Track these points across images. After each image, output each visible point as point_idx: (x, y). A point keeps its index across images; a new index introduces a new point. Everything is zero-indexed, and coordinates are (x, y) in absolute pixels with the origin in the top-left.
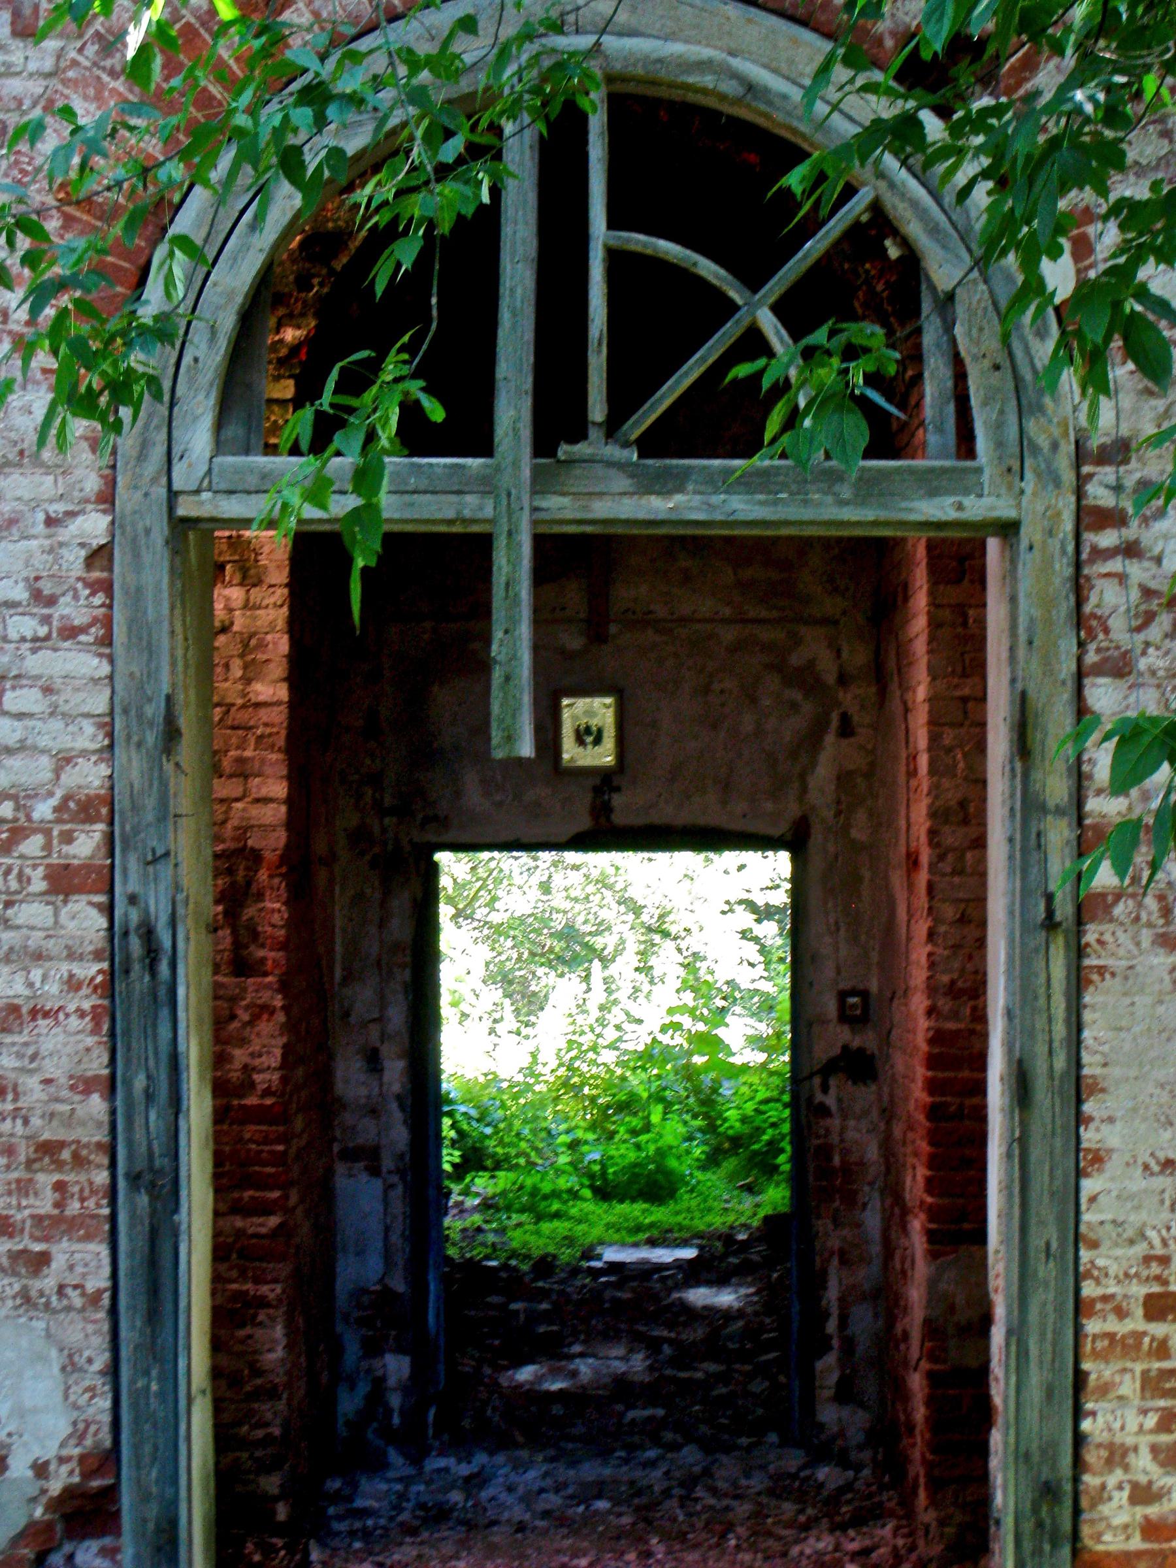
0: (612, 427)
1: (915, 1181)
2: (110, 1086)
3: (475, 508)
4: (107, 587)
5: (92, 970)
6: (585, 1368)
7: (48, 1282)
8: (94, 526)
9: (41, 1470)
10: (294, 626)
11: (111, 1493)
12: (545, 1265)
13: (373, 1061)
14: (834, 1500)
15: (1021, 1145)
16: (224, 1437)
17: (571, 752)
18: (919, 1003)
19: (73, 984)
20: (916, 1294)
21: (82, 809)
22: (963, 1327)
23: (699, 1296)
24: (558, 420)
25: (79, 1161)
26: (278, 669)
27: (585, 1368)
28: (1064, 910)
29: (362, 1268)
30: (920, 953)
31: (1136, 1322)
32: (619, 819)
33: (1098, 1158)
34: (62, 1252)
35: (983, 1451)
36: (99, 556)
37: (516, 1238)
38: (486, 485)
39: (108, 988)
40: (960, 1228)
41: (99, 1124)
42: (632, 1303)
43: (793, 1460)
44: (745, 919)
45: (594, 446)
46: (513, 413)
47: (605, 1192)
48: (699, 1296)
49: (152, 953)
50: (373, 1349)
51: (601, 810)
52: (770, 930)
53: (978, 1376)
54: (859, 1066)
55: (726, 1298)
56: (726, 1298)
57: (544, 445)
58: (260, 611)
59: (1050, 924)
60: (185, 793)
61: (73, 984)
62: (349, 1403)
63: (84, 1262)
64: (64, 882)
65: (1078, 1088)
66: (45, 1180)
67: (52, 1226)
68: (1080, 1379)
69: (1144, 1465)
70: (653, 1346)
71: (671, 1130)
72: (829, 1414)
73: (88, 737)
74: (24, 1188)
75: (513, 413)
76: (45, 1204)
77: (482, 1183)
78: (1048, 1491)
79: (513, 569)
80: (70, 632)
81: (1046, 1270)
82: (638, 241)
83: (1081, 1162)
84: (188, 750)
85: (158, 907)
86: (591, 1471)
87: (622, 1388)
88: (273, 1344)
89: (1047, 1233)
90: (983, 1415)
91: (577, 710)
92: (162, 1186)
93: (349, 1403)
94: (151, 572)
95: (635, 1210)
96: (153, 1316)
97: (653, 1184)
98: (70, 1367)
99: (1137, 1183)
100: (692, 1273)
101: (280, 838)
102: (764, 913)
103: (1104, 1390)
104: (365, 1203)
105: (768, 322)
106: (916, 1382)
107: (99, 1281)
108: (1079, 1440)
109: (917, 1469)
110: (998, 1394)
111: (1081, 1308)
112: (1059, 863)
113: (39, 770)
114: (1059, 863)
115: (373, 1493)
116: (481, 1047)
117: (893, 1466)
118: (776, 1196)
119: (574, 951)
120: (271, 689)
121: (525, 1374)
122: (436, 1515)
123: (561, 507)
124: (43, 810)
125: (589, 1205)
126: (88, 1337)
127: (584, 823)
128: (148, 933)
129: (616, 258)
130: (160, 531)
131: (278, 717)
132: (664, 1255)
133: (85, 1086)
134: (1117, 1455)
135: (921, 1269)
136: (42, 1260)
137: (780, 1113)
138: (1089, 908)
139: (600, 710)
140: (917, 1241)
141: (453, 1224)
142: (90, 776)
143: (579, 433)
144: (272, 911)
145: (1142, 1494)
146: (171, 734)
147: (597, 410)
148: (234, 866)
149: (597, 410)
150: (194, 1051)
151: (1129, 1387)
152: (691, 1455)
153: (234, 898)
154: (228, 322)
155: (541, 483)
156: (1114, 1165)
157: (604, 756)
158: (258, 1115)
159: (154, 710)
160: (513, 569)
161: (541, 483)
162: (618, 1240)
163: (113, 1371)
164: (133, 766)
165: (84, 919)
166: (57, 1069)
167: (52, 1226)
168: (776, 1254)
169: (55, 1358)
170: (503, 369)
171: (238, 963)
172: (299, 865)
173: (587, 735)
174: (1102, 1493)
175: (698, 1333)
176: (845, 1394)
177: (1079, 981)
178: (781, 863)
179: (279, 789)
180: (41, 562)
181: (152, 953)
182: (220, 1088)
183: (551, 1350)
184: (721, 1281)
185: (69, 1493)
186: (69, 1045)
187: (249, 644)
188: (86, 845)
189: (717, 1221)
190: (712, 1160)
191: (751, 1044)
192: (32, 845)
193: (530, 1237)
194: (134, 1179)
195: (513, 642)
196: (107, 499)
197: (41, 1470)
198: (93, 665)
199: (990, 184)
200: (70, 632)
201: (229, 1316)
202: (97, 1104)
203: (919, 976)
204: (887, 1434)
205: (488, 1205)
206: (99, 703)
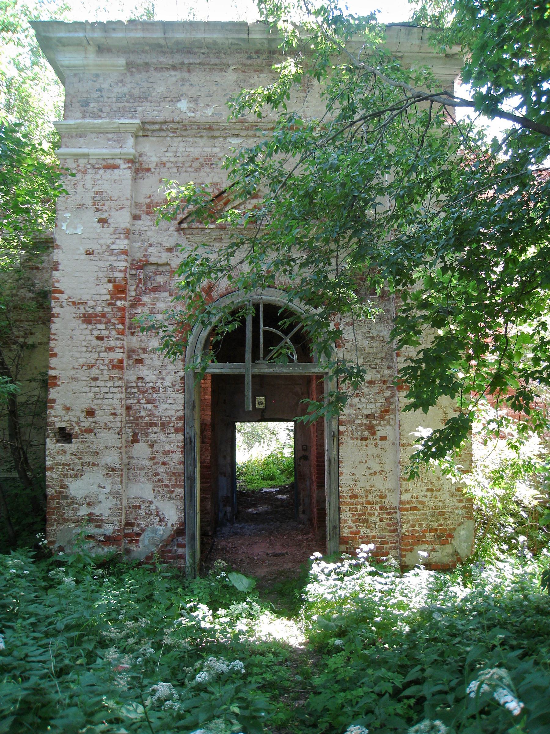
0: (264, 358)
1: (314, 477)
2: (184, 463)
3: (242, 371)
4: (184, 383)
5: (181, 445)
6: (260, 509)
7: (174, 495)
8: (182, 374)
9: (173, 525)
10: (212, 386)
11: (184, 529)
12: (253, 492)
13: (225, 457)
14: (302, 531)
15: (330, 471)
16: (202, 521)
17: (258, 406)
18: (315, 448)
19: (178, 447)
20: (315, 496)
21: (180, 419)
22: (322, 501)
23: (280, 496)
24: (255, 357)
25: (179, 475)
26: (210, 393)
27: (260, 509)
28: (336, 434)
29: (223, 492)
30: (315, 439)
31: (348, 500)
32: (266, 417)
33: (342, 473)
34: (176, 490)
35: (325, 521)
36: (183, 378)
37: (249, 487)
38: (244, 367)
39: (184, 447)
40: (321, 485)
41: (344, 511)
42: (267, 498)
43: (295, 524)
44: (287, 432)
45: (261, 361)
46: (248, 356)
47: (263, 479)
48: (280, 496)
49: (191, 442)
50: (225, 506)
51: (262, 416)
52: (292, 434)
53: (324, 509)
54: (305, 458)
55: (284, 497)
56: (284, 497)
57: (253, 361)
58: (208, 384)
59: (334, 436)
60: (197, 416)
61: (178, 447)
62: (221, 515)
63: (180, 492)
64: (177, 430)
65: (339, 462)
66: (173, 478)
67: (174, 486)
68: (340, 509)
69: (350, 523)
70: (272, 505)
71: (275, 469)
72: (301, 516)
73: (181, 407)
74: (170, 480)
75: (248, 356)
76: (173, 482)
77: (242, 478)
78: (335, 527)
79: (249, 381)
80: (178, 391)
81: (334, 491)
82: (268, 328)
83: (339, 474)
84: (197, 409)
85: (192, 434)
86: (261, 526)
87: (267, 512)
88: (209, 505)
89: (334, 485)
90: (325, 515)
91: (258, 399)
92: (193, 480)
93: (221, 515)
94: (191, 382)
95: (269, 482)
96: (191, 500)
97: (272, 478)
98: (178, 508)
99: (349, 477)
100: (279, 493)
101: (210, 421)
102: (290, 431)
103: (344, 511)
104: (223, 481)
105: (288, 341)
106: (315, 510)
107: (182, 495)
108: (340, 518)
109: (315, 525)
110: (327, 511)
111: (339, 497)
112: (335, 427)
113: (172, 413)
114: (335, 427)
115: (225, 530)
116: (242, 457)
117: (312, 524)
118: (292, 479)
119: (259, 438)
120: (208, 397)
121: (250, 510)
122: (236, 534)
123: (256, 371)
124: (173, 419)
125: (261, 481)
126: (180, 504)
127: (259, 418)
128: (190, 439)
129: (265, 332)
130: (192, 374)
131: (209, 401)
132: (274, 490)
133: (180, 463)
134: (346, 521)
135: (316, 492)
136: (173, 491)
137: (293, 465)
138: (340, 433)
139: (262, 399)
140: (315, 487)
141: (238, 485)
142: (181, 414)
143: (259, 359)
144: (209, 433)
145: (350, 527)
146: (194, 407)
147: (262, 355)
148: (203, 425)
149: (262, 355)
150: (197, 457)
151: (347, 510)
152: (278, 523)
153: (202, 431)
154: (203, 341)
155: (253, 367)
156: (344, 475)
157: (263, 407)
158: (206, 467)
159: (191, 403)
160: (249, 381)
161: (253, 367)
162: (265, 487)
163: (184, 509)
164: (188, 412)
165: (180, 437)
166: (176, 461)
167: (174, 486)
168: (292, 489)
169: (175, 507)
170: (247, 349)
171: (203, 442)
172: (213, 426)
173: (260, 403)
174: (343, 527)
175: (280, 503)
176: (304, 512)
177: (338, 445)
178: (292, 424)
179: (210, 413)
180: (173, 380)
181: (191, 442)
182: (201, 463)
183: (254, 506)
184: (283, 494)
185: (177, 529)
186: (177, 457)
187: (205, 389)
188: (180, 425)
189: (283, 484)
190: (282, 473)
191: (288, 452)
192: (172, 425)
193: (251, 487)
194: (188, 478)
195: (249, 392)
196: (183, 370)
197: (173, 525)
198: (182, 396)
199: (370, 212)
200: (178, 391)
201: (202, 500)
202: (182, 466)
203: (315, 443)
204: (310, 520)
205: (243, 481)
206: (182, 402)
